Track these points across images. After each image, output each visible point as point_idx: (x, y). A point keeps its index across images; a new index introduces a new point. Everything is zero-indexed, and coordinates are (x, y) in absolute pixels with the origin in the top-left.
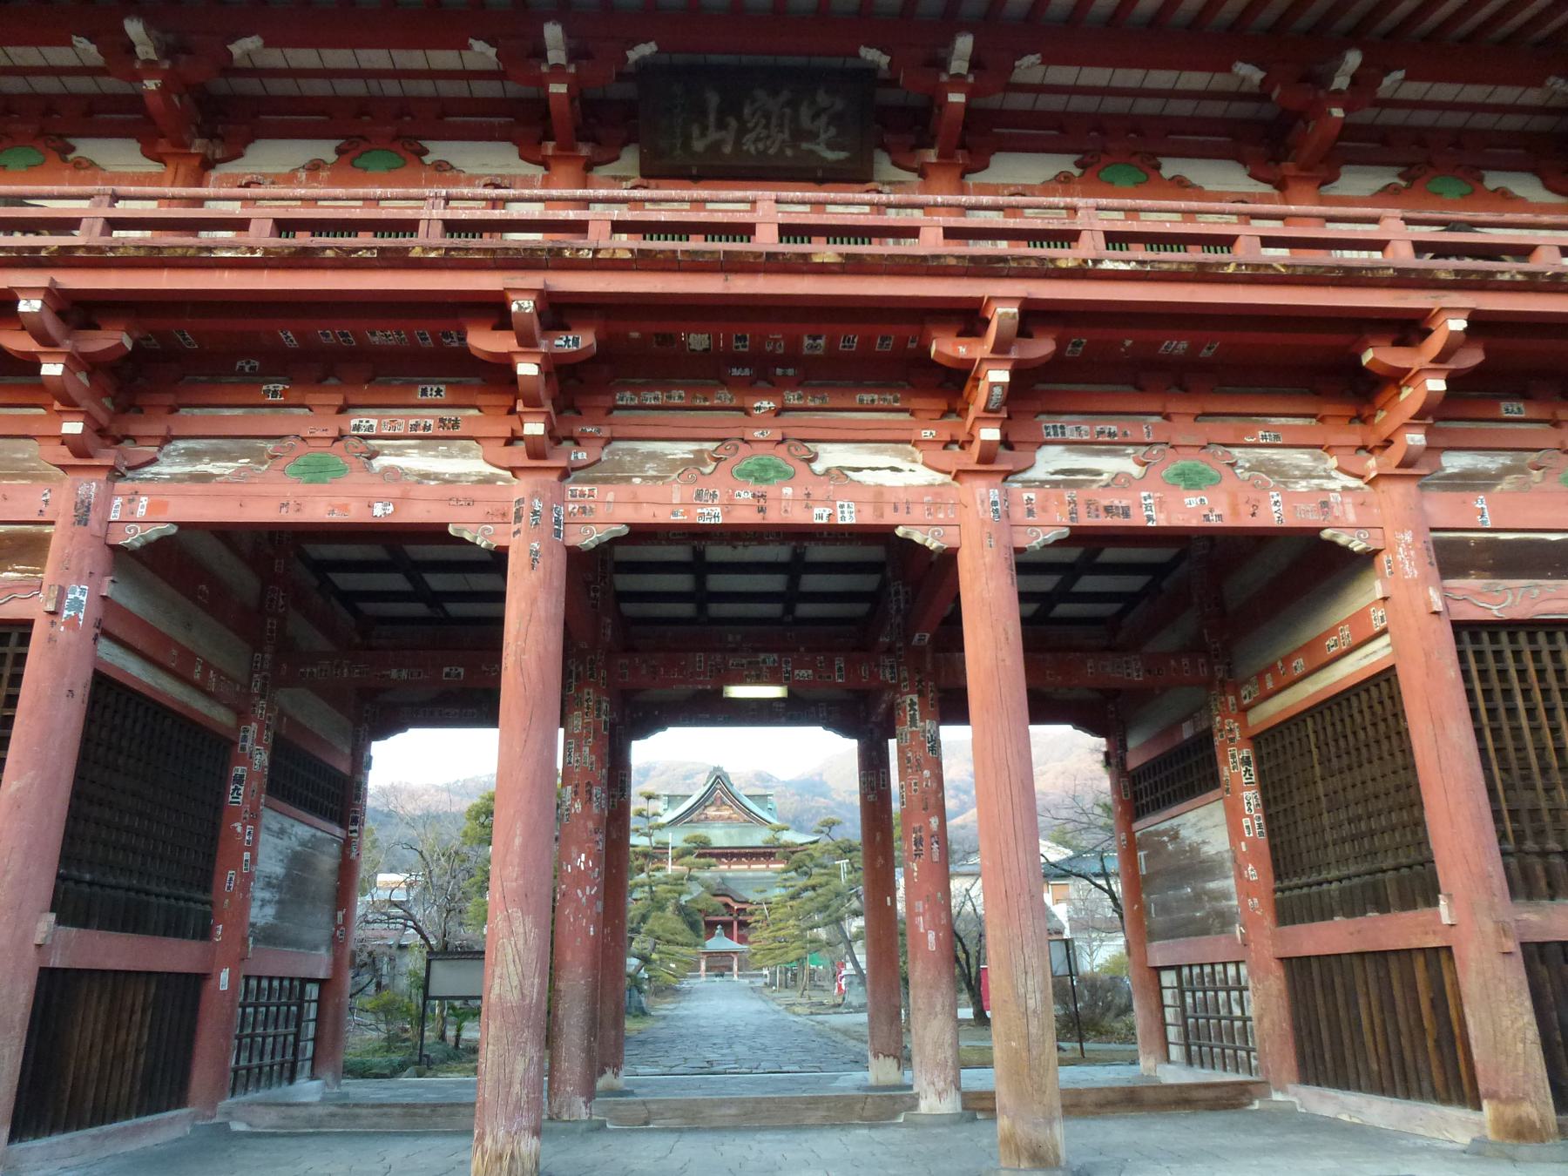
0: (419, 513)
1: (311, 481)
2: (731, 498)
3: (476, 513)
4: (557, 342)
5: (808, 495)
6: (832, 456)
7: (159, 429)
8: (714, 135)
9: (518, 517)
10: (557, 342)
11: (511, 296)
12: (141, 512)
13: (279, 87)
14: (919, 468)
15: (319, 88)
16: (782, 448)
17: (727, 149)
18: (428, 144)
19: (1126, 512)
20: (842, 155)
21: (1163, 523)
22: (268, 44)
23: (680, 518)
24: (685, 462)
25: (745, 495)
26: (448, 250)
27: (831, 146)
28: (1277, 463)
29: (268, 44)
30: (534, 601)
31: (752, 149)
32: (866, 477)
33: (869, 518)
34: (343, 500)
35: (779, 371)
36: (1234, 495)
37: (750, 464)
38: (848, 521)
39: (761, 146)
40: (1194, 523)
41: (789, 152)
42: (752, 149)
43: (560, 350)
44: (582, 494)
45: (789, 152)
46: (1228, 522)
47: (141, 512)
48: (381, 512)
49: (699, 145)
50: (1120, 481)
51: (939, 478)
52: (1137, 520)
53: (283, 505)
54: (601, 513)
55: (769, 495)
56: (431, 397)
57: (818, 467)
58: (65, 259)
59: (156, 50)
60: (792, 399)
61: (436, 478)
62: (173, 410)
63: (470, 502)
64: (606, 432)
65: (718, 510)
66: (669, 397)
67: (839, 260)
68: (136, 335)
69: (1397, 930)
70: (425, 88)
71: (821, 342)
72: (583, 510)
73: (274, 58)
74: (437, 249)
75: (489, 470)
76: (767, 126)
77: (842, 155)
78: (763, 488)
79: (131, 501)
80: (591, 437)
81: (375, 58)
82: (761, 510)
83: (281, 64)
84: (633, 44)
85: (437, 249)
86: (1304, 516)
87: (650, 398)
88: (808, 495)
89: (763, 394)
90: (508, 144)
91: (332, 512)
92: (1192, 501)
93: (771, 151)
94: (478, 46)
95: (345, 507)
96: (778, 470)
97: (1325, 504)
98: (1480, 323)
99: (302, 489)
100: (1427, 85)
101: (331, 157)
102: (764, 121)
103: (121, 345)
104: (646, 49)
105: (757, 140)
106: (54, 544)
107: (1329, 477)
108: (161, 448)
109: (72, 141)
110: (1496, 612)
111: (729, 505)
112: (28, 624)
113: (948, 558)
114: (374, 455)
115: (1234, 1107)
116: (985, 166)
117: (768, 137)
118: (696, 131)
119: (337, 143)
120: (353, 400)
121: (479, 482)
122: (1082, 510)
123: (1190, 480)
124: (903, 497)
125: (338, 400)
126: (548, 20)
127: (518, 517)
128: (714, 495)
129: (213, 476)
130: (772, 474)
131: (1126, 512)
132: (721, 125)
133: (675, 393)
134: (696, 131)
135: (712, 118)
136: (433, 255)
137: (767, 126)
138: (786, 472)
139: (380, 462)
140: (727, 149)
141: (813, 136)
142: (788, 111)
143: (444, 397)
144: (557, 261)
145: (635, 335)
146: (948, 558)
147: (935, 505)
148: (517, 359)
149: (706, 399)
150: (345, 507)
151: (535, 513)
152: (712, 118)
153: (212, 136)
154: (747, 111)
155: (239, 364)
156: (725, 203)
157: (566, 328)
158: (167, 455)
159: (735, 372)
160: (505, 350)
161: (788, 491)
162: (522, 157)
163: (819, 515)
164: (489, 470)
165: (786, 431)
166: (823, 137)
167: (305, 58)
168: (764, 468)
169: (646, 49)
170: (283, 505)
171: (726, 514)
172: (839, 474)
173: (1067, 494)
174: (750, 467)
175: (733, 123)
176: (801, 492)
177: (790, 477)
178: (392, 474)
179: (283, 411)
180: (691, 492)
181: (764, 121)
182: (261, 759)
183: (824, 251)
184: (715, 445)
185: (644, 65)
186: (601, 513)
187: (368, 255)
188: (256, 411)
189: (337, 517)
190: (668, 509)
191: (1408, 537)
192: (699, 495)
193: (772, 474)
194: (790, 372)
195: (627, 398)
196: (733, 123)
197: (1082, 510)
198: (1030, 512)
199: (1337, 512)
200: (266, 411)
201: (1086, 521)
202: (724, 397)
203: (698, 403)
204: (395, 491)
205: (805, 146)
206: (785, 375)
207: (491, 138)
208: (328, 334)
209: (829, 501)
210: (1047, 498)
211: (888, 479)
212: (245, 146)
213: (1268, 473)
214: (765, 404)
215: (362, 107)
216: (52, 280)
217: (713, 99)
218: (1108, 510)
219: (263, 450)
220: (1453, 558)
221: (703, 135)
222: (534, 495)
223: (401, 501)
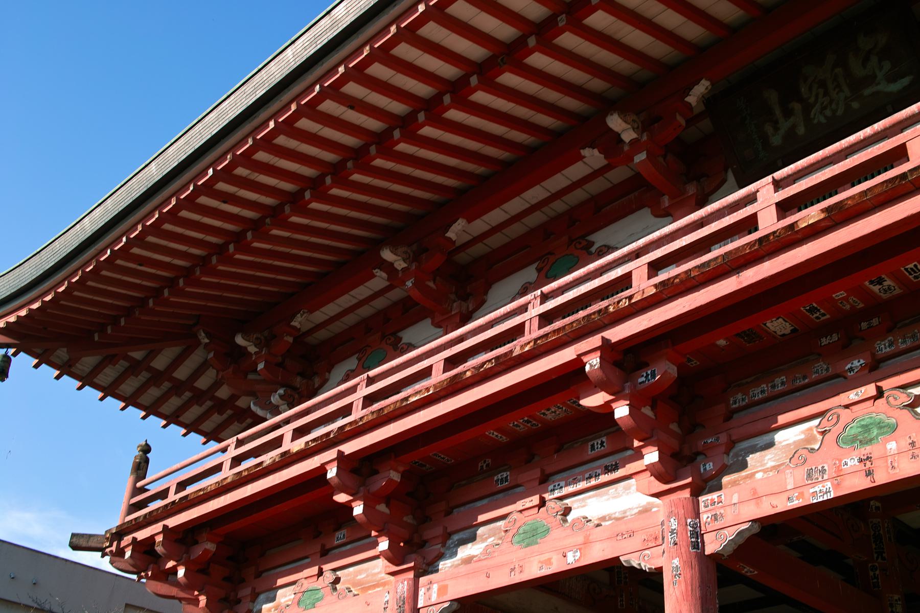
1: (528, 545)
2: (839, 469)
4: (640, 380)
5: (913, 444)
7: (438, 531)
8: (785, 125)
10: (640, 380)
11: (585, 359)
13: (497, 241)
15: (517, 230)
16: (880, 402)
17: (801, 130)
22: (470, 221)
23: (796, 503)
25: (852, 462)
26: (536, 340)
27: (891, 79)
29: (470, 221)
31: (823, 120)
34: (546, 556)
35: (864, 325)
39: (828, 113)
41: (855, 105)
42: (823, 120)
43: (643, 386)
44: (713, 503)
45: (855, 105)
47: (434, 599)
49: (776, 140)
53: (513, 570)
55: (874, 456)
56: (599, 450)
59: (404, 261)
60: (883, 347)
61: (610, 519)
62: (449, 512)
64: (723, 438)
65: (829, 485)
66: (773, 387)
67: (822, 216)
68: (401, 469)
70: (579, 195)
71: (888, 282)
72: (715, 517)
73: (480, 226)
74: (529, 343)
76: (826, 94)
77: (906, 81)
78: (866, 450)
79: (429, 589)
80: (712, 447)
81: (535, 194)
82: (869, 473)
83: (486, 228)
84: (687, 91)
85: (529, 343)
87: (757, 393)
88: (913, 444)
89: (854, 356)
91: (541, 568)
93: (840, 112)
94: (586, 152)
95: (548, 562)
96: (880, 425)
99: (522, 553)
100: (534, 112)
102: (821, 91)
103: (391, 481)
104: (702, 88)
105: (824, 108)
108: (444, 544)
114: (567, 511)
117: (831, 102)
118: (769, 129)
119: (535, 265)
120: (549, 470)
121: (640, 512)
125: (536, 473)
126: (606, 116)
128: (823, 471)
130: (875, 432)
132: (788, 113)
133: (778, 381)
134: (769, 129)
135: (778, 112)
136: (527, 349)
137: (826, 94)
138: (888, 426)
140: (801, 130)
141: (871, 79)
142: (838, 70)
143: (607, 447)
145: (722, 342)
148: (614, 405)
149: (804, 377)
151: (672, 532)
152: (778, 112)
153: (464, 298)
154: (803, 90)
155: (480, 465)
156: (717, 212)
157: (646, 365)
158: (449, 548)
159: (824, 341)
160: (601, 402)
161: (892, 446)
165: (879, 384)
166: (880, 75)
167: (496, 216)
168: (866, 428)
169: (702, 88)
170: (513, 570)
171: (837, 486)
174: (853, 432)
175: (797, 106)
176: (905, 443)
179: (510, 492)
181: (821, 91)
183: (812, 214)
184: (816, 422)
185: (708, 100)
187: (490, 366)
188: (495, 497)
190: (784, 496)
192: (809, 476)
193: (875, 432)
194: (875, 322)
195: (738, 399)
196: (797, 106)
200: (500, 495)
202: (821, 368)
203: (799, 383)
205: (867, 92)
206: (870, 327)
207: (632, 212)
208: (519, 423)
212: (486, 293)
214: (856, 363)
215: (545, 231)
216: (339, 451)
217: (772, 97)
219: (499, 528)
221: (776, 129)
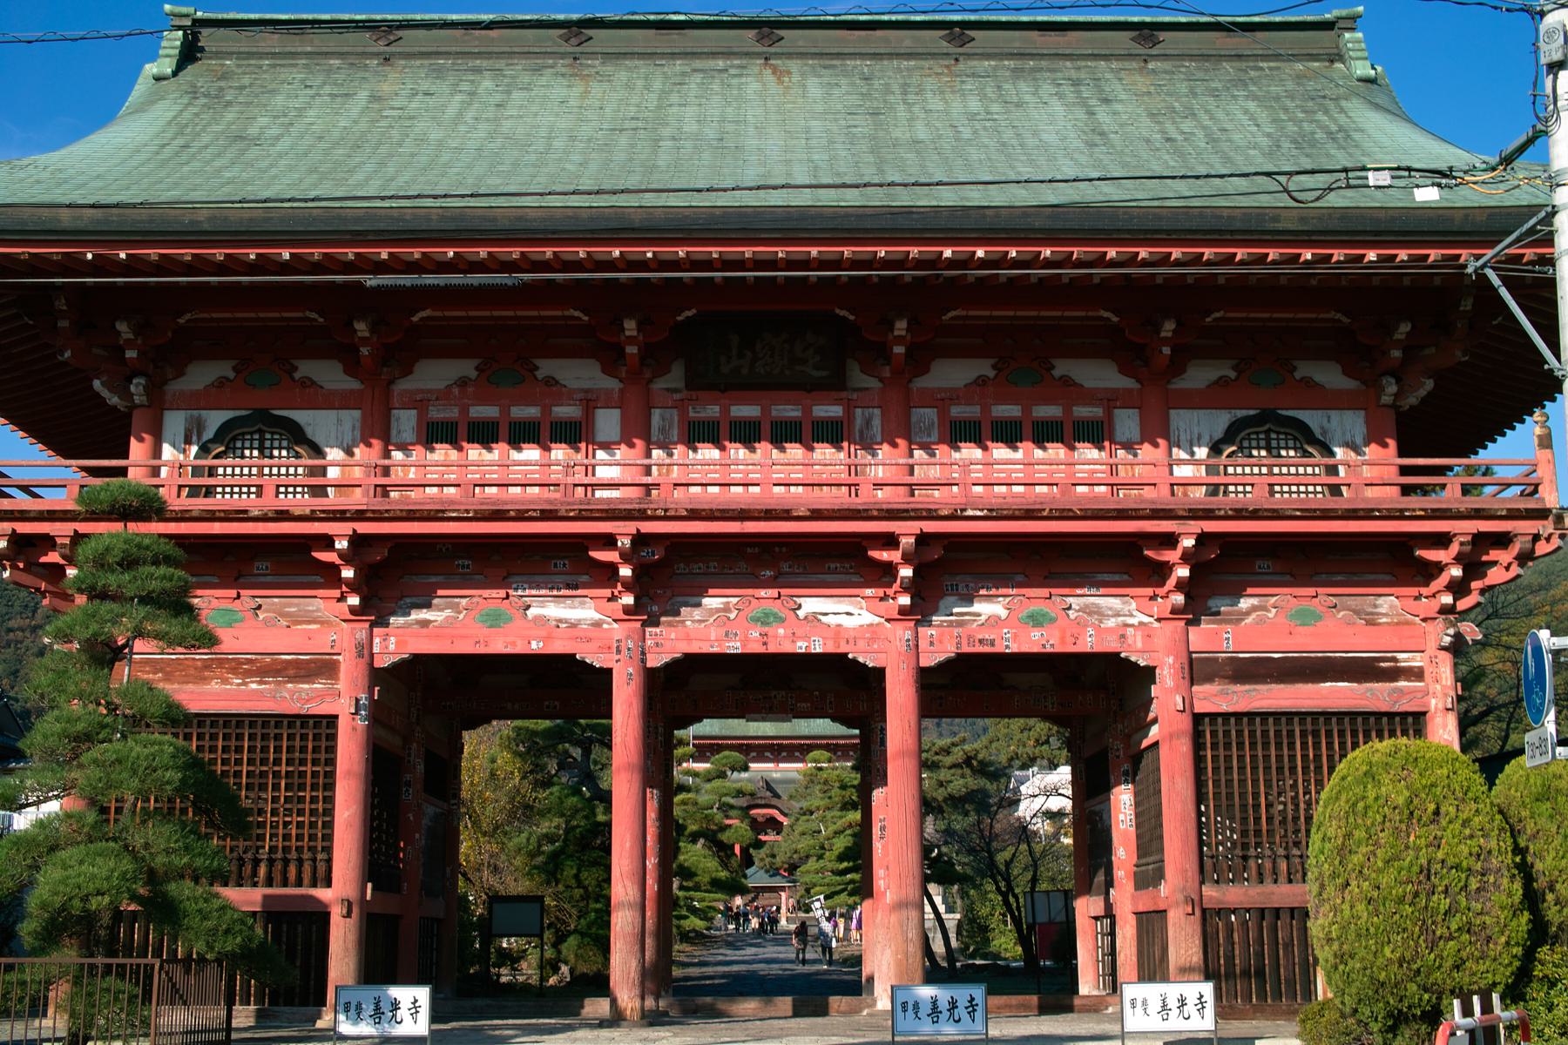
0: (559, 647)
3: (593, 646)
6: (811, 605)
9: (619, 652)
12: (392, 647)
14: (864, 612)
17: (745, 371)
18: (538, 362)
19: (992, 643)
20: (824, 373)
21: (1016, 650)
23: (715, 650)
24: (718, 610)
28: (1097, 606)
30: (631, 705)
32: (831, 620)
33: (831, 648)
36: (1063, 631)
37: (757, 612)
38: (818, 650)
40: (1035, 650)
46: (1058, 649)
48: (535, 646)
50: (994, 621)
51: (877, 620)
52: (999, 648)
54: (668, 645)
57: (801, 613)
58: (360, 516)
60: (785, 567)
63: (589, 640)
69: (1280, 894)
75: (597, 616)
77: (824, 373)
78: (766, 629)
82: (765, 644)
86: (1110, 645)
90: (592, 361)
92: (1036, 635)
97: (1123, 636)
98: (1202, 538)
101: (473, 374)
106: (343, 668)
107: (1131, 615)
109: (296, 362)
110: (1224, 707)
111: (745, 641)
112: (332, 720)
113: (880, 673)
115: (1096, 1011)
116: (926, 370)
122: (964, 642)
123: (1036, 620)
124: (852, 634)
127: (619, 652)
129: (430, 622)
131: (992, 643)
139: (531, 613)
140: (745, 371)
144: (642, 515)
146: (880, 673)
147: (873, 640)
150: (514, 644)
161: (781, 631)
162: (603, 372)
163: (801, 647)
164: (597, 616)
172: (814, 618)
173: (956, 631)
177: (781, 621)
178: (541, 620)
180: (722, 631)
182: (420, 768)
186: (668, 645)
189: (509, 650)
191: (1171, 660)
192: (727, 635)
197: (964, 642)
198: (932, 643)
199: (1130, 641)
201: (966, 649)
204: (544, 633)
209: (806, 638)
210: (942, 635)
211: (847, 622)
213: (1089, 614)
218: (981, 641)
220: (1198, 670)
222: (628, 637)
223: (547, 639)
